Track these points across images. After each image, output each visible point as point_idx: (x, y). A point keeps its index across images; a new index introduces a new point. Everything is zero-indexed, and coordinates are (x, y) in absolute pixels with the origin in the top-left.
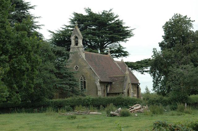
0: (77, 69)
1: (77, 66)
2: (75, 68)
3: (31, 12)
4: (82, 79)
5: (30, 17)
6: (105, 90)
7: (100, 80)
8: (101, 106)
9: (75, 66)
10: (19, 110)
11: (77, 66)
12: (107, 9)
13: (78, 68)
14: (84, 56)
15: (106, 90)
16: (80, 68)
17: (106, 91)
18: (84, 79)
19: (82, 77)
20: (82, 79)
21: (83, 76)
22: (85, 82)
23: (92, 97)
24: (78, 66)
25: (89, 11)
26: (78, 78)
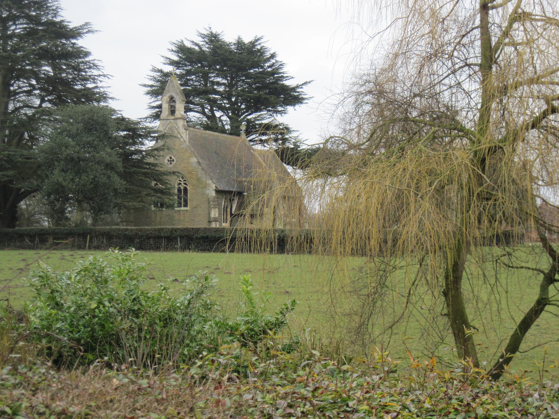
0: (171, 163)
1: (171, 158)
2: (168, 161)
3: (81, 42)
4: (180, 184)
5: (80, 53)
6: (227, 207)
7: (216, 187)
8: (37, 239)
9: (168, 158)
10: (18, 244)
11: (171, 158)
12: (219, 32)
13: (173, 161)
14: (187, 137)
15: (229, 207)
16: (177, 161)
17: (229, 210)
18: (185, 184)
19: (181, 179)
20: (180, 184)
21: (183, 178)
22: (185, 189)
23: (200, 223)
24: (173, 158)
25: (213, 39)
26: (174, 183)
